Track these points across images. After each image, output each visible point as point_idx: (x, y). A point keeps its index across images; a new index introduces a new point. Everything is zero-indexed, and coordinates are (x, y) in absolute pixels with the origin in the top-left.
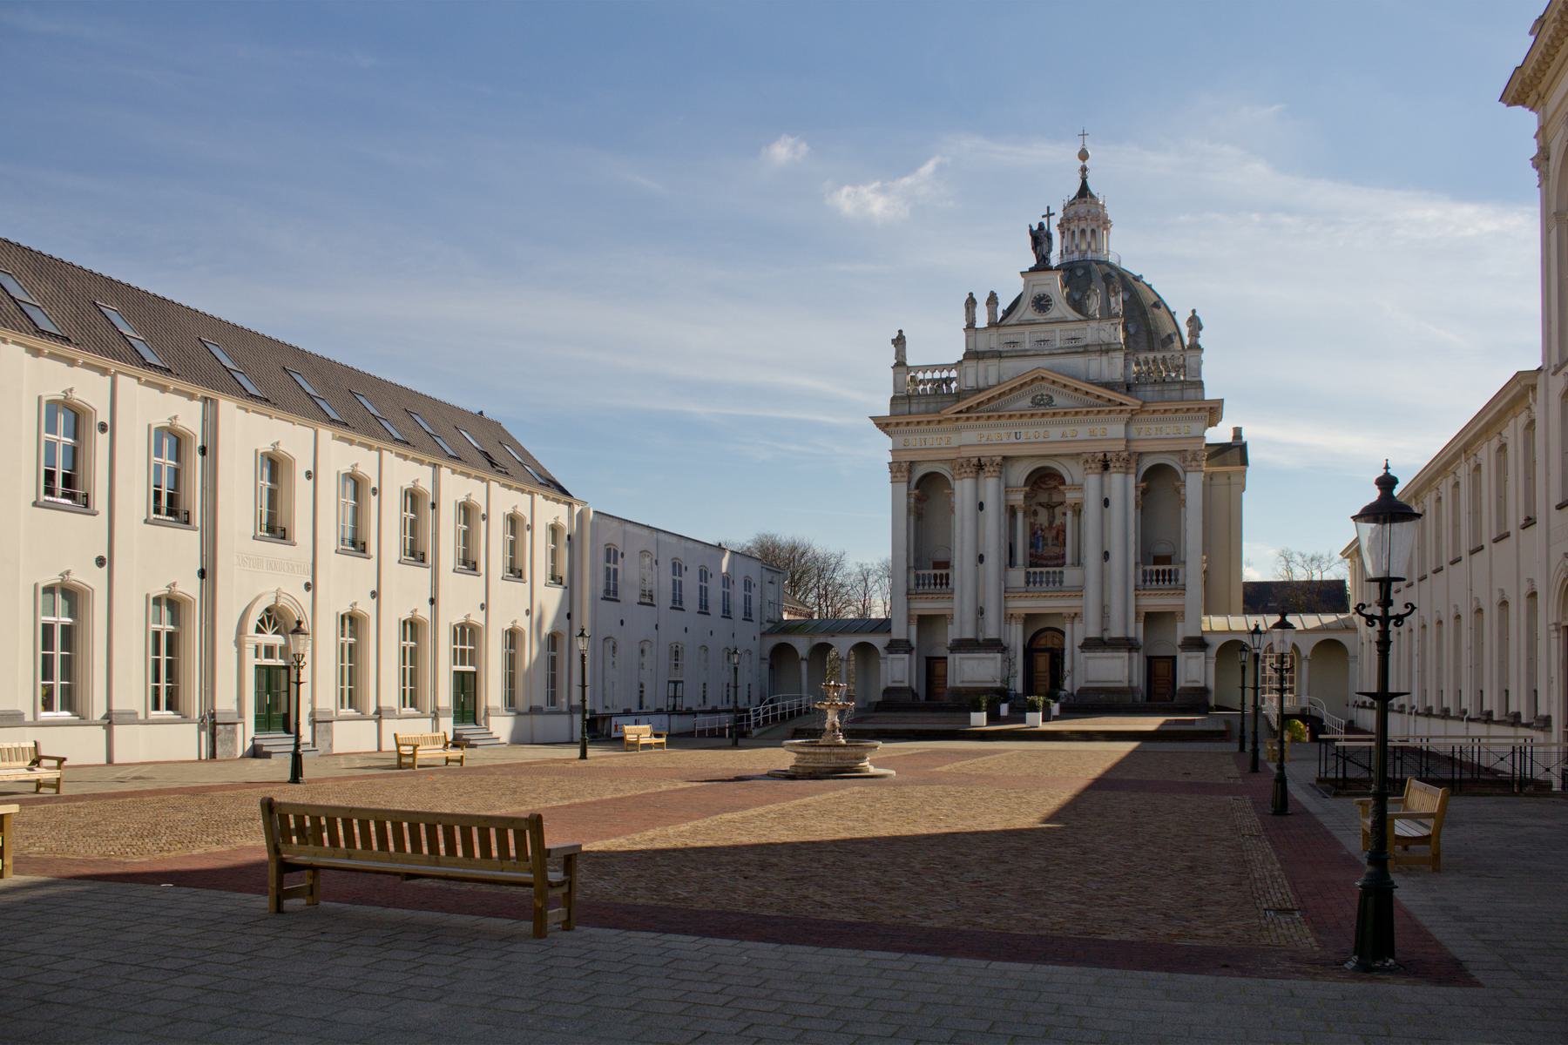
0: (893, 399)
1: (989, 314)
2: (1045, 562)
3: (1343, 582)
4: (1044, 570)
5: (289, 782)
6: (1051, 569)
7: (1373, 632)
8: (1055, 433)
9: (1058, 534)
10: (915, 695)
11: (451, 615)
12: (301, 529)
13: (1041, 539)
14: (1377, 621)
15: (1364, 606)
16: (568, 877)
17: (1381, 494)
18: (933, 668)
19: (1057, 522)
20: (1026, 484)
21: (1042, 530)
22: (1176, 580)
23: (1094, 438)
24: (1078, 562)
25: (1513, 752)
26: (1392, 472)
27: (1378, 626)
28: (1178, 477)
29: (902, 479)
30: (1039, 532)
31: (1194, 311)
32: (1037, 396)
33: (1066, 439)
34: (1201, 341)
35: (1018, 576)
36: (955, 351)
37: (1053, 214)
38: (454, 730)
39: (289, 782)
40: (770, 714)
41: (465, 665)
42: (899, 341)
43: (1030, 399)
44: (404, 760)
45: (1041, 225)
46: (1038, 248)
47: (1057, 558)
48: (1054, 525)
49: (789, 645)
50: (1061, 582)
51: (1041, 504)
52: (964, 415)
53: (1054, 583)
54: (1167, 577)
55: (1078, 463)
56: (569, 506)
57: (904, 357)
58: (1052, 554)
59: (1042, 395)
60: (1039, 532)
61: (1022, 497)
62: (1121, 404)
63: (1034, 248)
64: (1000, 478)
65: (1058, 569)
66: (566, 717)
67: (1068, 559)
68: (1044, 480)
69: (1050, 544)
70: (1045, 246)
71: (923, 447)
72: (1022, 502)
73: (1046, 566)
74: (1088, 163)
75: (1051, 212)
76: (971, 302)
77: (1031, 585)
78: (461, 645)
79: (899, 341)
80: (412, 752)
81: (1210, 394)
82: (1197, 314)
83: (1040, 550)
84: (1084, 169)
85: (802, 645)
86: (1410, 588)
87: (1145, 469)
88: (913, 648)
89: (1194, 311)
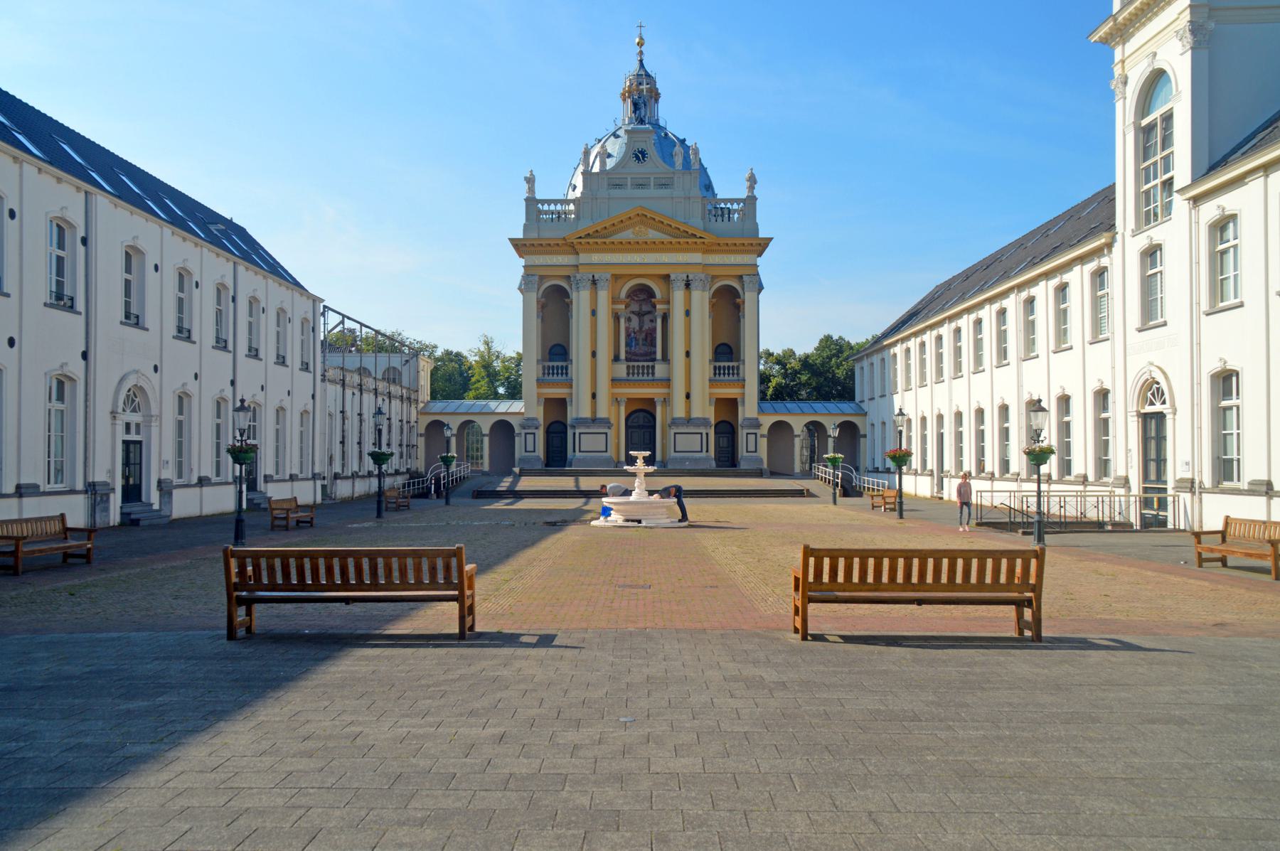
2: (637, 358)
4: (636, 364)
6: (641, 364)
9: (646, 336)
12: (150, 319)
13: (634, 340)
16: (248, 618)
21: (635, 333)
22: (738, 374)
24: (666, 358)
25: (679, 493)
30: (633, 334)
31: (752, 169)
34: (756, 193)
35: (621, 369)
42: (530, 181)
46: (638, 112)
47: (646, 354)
48: (644, 329)
50: (653, 374)
51: (633, 312)
53: (648, 374)
58: (641, 352)
60: (633, 334)
62: (701, 237)
65: (560, 364)
66: (311, 483)
67: (659, 356)
68: (643, 294)
73: (638, 361)
74: (643, 48)
79: (530, 181)
81: (763, 234)
83: (633, 349)
88: (612, 425)
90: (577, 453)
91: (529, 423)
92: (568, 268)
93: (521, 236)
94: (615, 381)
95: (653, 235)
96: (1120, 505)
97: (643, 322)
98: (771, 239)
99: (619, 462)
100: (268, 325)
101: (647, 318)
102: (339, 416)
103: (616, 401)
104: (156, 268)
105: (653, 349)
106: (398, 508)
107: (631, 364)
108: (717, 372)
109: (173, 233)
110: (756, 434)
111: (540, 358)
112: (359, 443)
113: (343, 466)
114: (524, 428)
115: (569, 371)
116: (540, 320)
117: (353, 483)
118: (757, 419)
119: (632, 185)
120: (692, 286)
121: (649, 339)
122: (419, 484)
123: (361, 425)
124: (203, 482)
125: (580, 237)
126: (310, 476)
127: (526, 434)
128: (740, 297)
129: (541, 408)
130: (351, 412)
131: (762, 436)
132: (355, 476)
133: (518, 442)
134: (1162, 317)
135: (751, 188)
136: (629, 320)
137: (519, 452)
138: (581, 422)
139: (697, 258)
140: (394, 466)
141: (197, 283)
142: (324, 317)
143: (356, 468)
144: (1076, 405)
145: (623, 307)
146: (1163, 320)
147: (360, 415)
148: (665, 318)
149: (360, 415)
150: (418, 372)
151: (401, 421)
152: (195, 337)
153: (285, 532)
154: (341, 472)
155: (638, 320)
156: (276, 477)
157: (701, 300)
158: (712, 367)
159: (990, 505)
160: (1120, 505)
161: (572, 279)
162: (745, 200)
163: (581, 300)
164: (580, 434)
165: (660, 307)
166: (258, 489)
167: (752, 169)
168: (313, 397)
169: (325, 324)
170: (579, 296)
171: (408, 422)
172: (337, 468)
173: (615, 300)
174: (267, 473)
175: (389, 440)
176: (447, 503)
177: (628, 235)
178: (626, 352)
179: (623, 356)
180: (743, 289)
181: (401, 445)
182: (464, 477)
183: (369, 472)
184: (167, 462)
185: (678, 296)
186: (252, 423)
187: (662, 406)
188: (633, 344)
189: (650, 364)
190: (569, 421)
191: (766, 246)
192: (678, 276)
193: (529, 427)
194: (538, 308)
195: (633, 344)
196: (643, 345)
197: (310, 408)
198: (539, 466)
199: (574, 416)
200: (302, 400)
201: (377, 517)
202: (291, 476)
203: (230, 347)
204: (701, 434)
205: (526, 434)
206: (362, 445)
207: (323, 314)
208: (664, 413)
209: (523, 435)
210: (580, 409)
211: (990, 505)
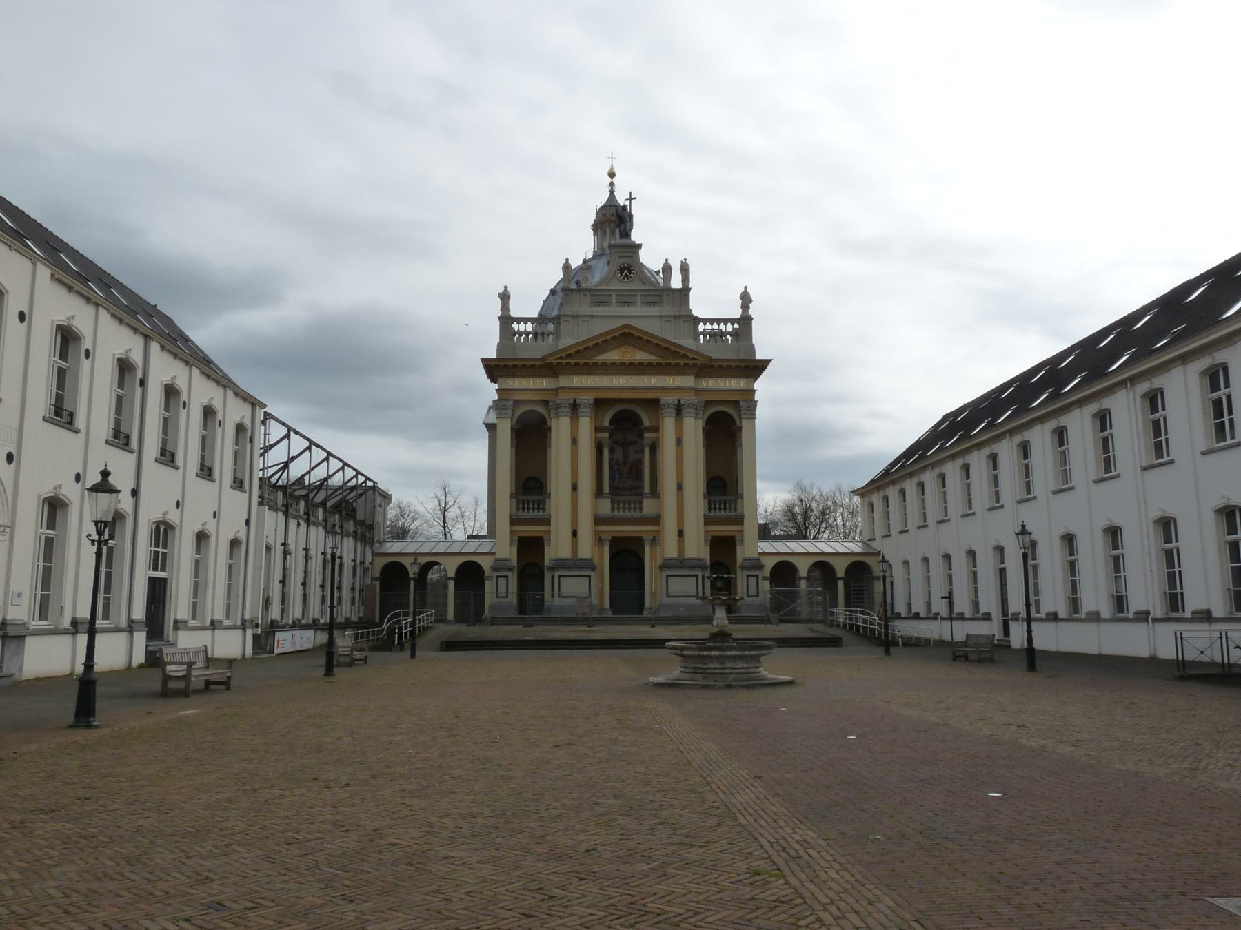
5: (70, 727)
7: (95, 548)
10: (602, 610)
11: (150, 512)
14: (96, 543)
15: (90, 535)
17: (100, 482)
19: (631, 458)
21: (618, 465)
24: (655, 493)
26: (108, 468)
27: (96, 545)
30: (616, 466)
31: (746, 288)
34: (751, 312)
37: (635, 198)
38: (147, 646)
39: (70, 727)
41: (157, 571)
44: (172, 685)
50: (641, 509)
52: (564, 361)
55: (1127, 388)
56: (252, 407)
57: (508, 310)
62: (693, 358)
65: (536, 498)
67: (647, 489)
74: (614, 180)
77: (712, 511)
78: (162, 548)
80: (184, 673)
83: (616, 482)
84: (612, 184)
86: (922, 530)
89: (746, 288)
90: (557, 599)
91: (499, 566)
92: (545, 392)
94: (599, 521)
95: (640, 356)
96: (754, 673)
98: (769, 361)
99: (603, 609)
100: (190, 426)
102: (280, 549)
103: (599, 540)
104: (22, 317)
106: (352, 663)
109: (52, 275)
110: (757, 576)
111: (514, 491)
112: (304, 584)
113: (283, 611)
114: (496, 571)
115: (547, 506)
116: (514, 450)
118: (758, 559)
120: (684, 411)
122: (373, 635)
123: (307, 562)
125: (561, 358)
126: (239, 623)
127: (498, 577)
130: (296, 546)
131: (764, 578)
132: (296, 625)
133: (489, 586)
134: (1115, 470)
136: (612, 451)
137: (489, 598)
138: (560, 565)
139: (688, 381)
140: (344, 614)
141: (87, 352)
142: (265, 425)
143: (298, 615)
144: (1082, 544)
145: (607, 435)
146: (1034, 495)
147: (306, 549)
148: (654, 447)
149: (306, 549)
150: (375, 506)
151: (354, 561)
152: (80, 422)
153: (186, 699)
154: (279, 619)
156: (192, 623)
157: (693, 428)
160: (754, 673)
161: (551, 404)
162: (738, 319)
163: (560, 428)
164: (560, 576)
166: (165, 638)
168: (247, 522)
169: (265, 434)
170: (341, 647)
171: (362, 563)
172: (275, 613)
173: (598, 429)
174: (179, 617)
176: (413, 655)
177: (614, 356)
178: (611, 487)
179: (606, 489)
180: (740, 416)
181: (353, 589)
182: (427, 627)
183: (314, 620)
184: (19, 595)
185: (668, 424)
186: (160, 550)
187: (651, 546)
188: (617, 476)
189: (637, 498)
190: (547, 562)
192: (668, 399)
193: (501, 569)
194: (512, 437)
195: (617, 476)
197: (243, 536)
198: (513, 614)
199: (553, 556)
200: (231, 526)
201: (325, 675)
202: (213, 622)
203: (134, 444)
204: (697, 576)
205: (498, 577)
206: (307, 586)
207: (263, 423)
208: (653, 556)
209: (494, 578)
210: (558, 548)
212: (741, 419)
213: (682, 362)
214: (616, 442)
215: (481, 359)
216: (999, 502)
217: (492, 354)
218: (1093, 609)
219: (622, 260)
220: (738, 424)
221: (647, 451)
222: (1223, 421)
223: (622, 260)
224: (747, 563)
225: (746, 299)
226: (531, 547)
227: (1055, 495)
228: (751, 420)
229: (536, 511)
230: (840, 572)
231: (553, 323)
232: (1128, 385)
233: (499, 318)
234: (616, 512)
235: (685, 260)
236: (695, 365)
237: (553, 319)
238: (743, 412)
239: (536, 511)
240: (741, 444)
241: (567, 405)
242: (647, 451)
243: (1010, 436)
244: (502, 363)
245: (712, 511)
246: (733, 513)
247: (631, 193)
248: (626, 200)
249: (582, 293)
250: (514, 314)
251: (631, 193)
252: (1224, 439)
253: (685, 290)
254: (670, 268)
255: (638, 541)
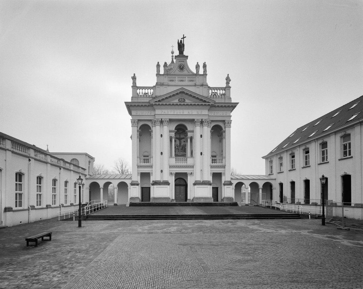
0: (132, 97)
1: (164, 70)
3: (320, 144)
8: (186, 112)
9: (182, 148)
18: (146, 192)
19: (182, 144)
20: (175, 129)
23: (198, 114)
28: (150, 129)
29: (135, 126)
31: (228, 75)
32: (180, 99)
33: (190, 114)
36: (152, 81)
37: (185, 37)
40: (93, 208)
42: (134, 78)
43: (178, 100)
45: (181, 41)
48: (181, 145)
49: (97, 183)
52: (157, 103)
54: (215, 161)
57: (135, 83)
59: (182, 99)
61: (174, 134)
62: (208, 102)
63: (179, 49)
64: (160, 126)
69: (180, 151)
70: (182, 48)
71: (142, 115)
72: (174, 136)
75: (184, 37)
76: (158, 66)
79: (134, 78)
82: (229, 76)
85: (101, 183)
87: (185, 124)
89: (198, 63)
93: (130, 101)
97: (181, 142)
98: (238, 103)
101: (182, 140)
105: (185, 153)
107: (177, 158)
108: (213, 161)
117: (29, 220)
119: (178, 81)
121: (183, 149)
124: (33, 208)
128: (151, 129)
129: (139, 177)
135: (228, 83)
136: (175, 141)
155: (179, 141)
157: (207, 131)
158: (211, 159)
159: (342, 216)
163: (156, 130)
165: (189, 135)
167: (228, 75)
173: (170, 131)
175: (39, 188)
191: (235, 106)
196: (181, 151)
211: (342, 216)
212: (225, 128)
213: (204, 104)
214: (177, 138)
215: (125, 102)
216: (350, 155)
217: (129, 100)
218: (314, 201)
219: (180, 63)
220: (224, 129)
221: (189, 140)
222: (347, 151)
223: (180, 63)
224: (226, 183)
225: (228, 80)
226: (145, 176)
227: (303, 169)
228: (229, 128)
229: (147, 163)
230: (261, 186)
231: (153, 89)
232: (316, 141)
233: (132, 86)
234: (177, 163)
235: (205, 63)
236: (209, 105)
237: (153, 87)
238: (226, 124)
239: (147, 163)
240: (225, 138)
241: (159, 121)
242: (189, 140)
243: (335, 134)
244: (133, 104)
245: (213, 163)
246: (221, 164)
247: (184, 35)
248: (182, 39)
249: (164, 87)
250: (138, 85)
251: (184, 35)
252: (346, 156)
253: (205, 75)
254: (199, 66)
255: (186, 174)
